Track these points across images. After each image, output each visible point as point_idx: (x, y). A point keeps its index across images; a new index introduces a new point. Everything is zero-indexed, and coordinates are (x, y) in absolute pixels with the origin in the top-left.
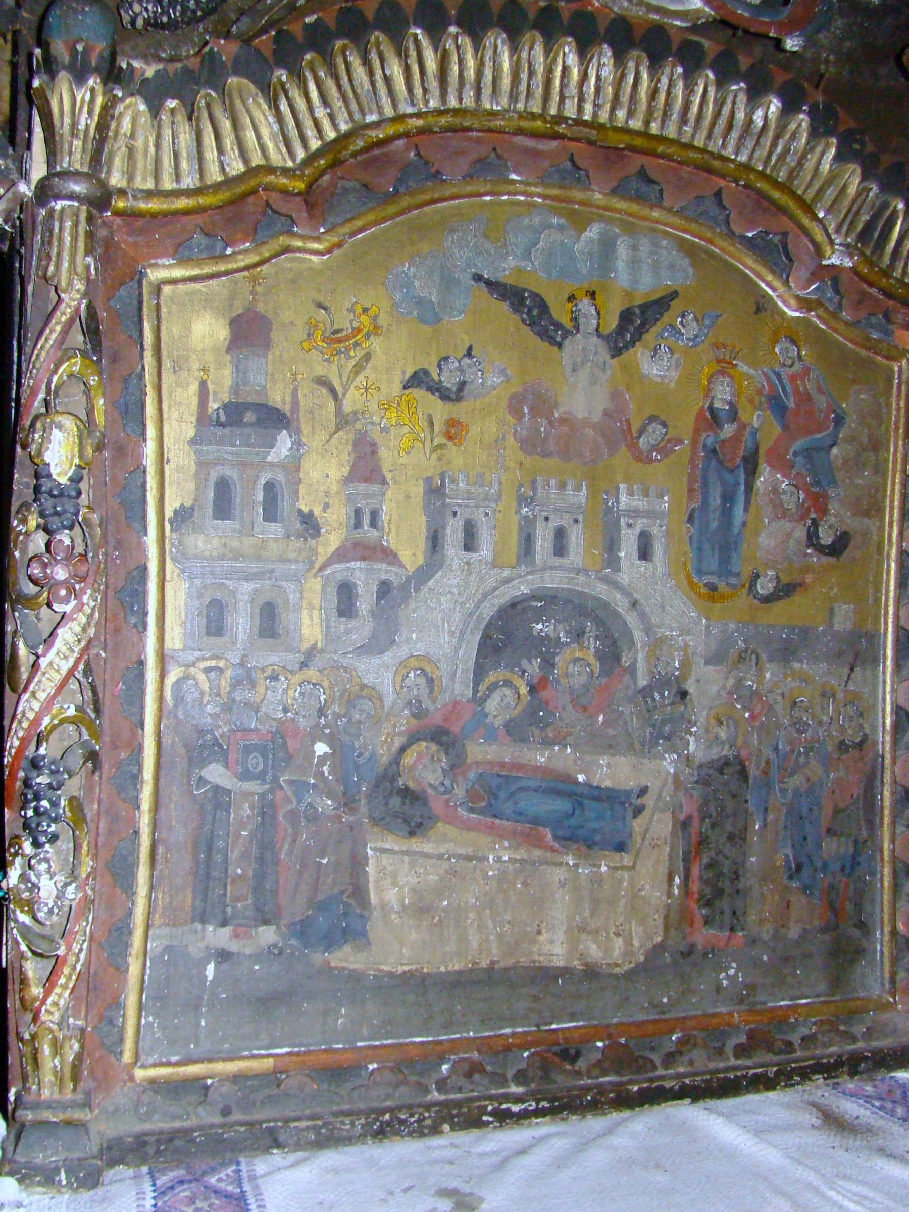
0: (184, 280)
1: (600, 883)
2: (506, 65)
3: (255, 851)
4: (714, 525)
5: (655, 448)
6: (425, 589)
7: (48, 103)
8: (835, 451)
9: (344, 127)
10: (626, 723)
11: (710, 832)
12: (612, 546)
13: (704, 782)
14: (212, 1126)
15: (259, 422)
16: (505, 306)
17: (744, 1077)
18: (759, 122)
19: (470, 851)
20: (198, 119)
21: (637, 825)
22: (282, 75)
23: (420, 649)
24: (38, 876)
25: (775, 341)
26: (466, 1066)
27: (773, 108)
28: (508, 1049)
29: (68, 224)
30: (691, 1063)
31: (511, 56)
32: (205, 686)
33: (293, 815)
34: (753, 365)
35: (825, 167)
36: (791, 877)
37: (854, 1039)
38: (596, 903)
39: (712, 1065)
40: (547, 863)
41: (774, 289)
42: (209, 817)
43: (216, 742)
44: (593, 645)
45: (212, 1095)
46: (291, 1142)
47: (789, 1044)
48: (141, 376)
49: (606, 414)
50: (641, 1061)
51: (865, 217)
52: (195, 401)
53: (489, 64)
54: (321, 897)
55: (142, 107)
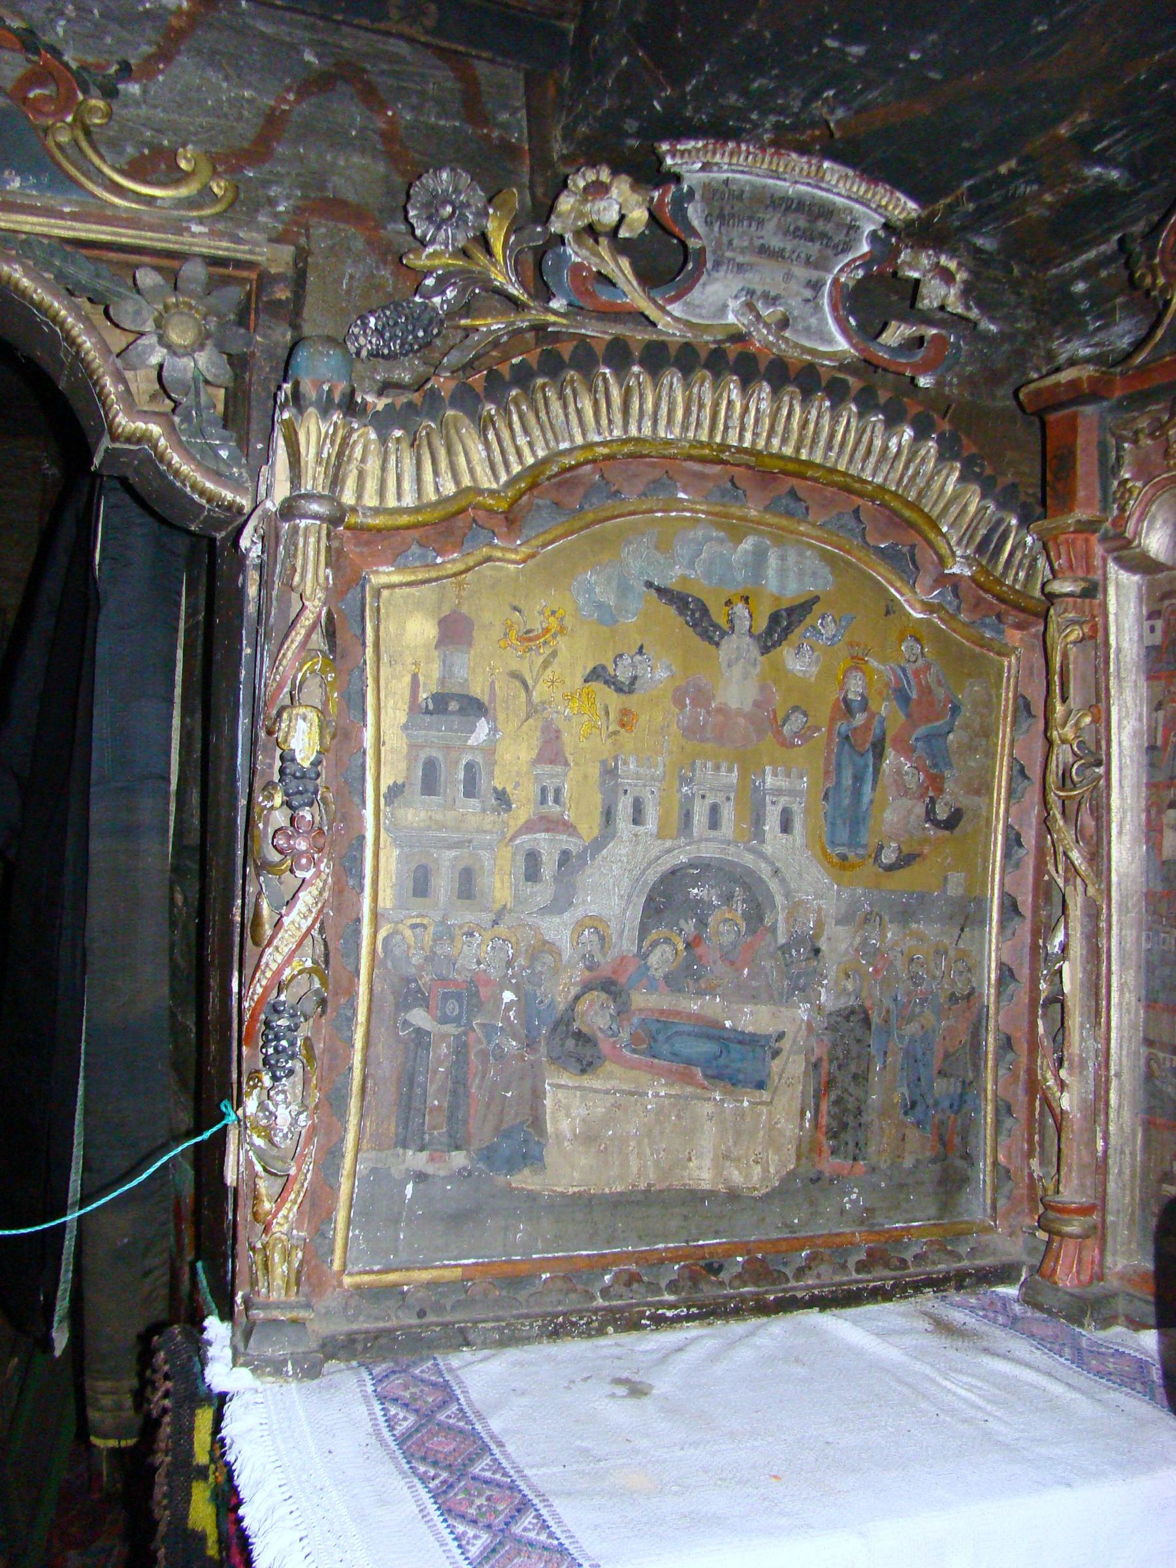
0: (402, 585)
1: (743, 1116)
2: (680, 399)
3: (450, 1085)
4: (846, 802)
5: (797, 734)
6: (599, 858)
7: (296, 434)
8: (951, 736)
9: (541, 454)
10: (767, 975)
11: (837, 1073)
12: (758, 820)
13: (832, 1028)
14: (411, 1326)
15: (462, 711)
16: (672, 610)
17: (865, 1289)
18: (894, 449)
19: (632, 1087)
20: (419, 446)
21: (776, 1065)
22: (491, 408)
23: (594, 910)
24: (276, 1105)
25: (902, 640)
26: (625, 1277)
27: (906, 437)
28: (662, 1261)
29: (312, 540)
30: (819, 1276)
31: (684, 392)
32: (412, 941)
33: (484, 1054)
34: (883, 661)
35: (950, 489)
36: (906, 1113)
37: (959, 1258)
38: (738, 1134)
39: (837, 1279)
40: (699, 1098)
41: (902, 595)
42: (412, 1055)
43: (419, 990)
44: (740, 907)
45: (410, 1300)
46: (479, 1341)
47: (903, 1261)
48: (363, 670)
49: (757, 704)
50: (775, 1275)
51: (983, 531)
52: (407, 692)
53: (665, 398)
54: (505, 1126)
55: (373, 436)
